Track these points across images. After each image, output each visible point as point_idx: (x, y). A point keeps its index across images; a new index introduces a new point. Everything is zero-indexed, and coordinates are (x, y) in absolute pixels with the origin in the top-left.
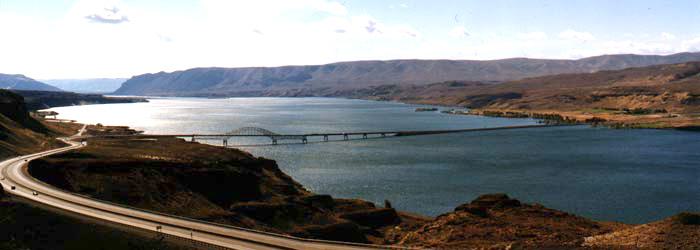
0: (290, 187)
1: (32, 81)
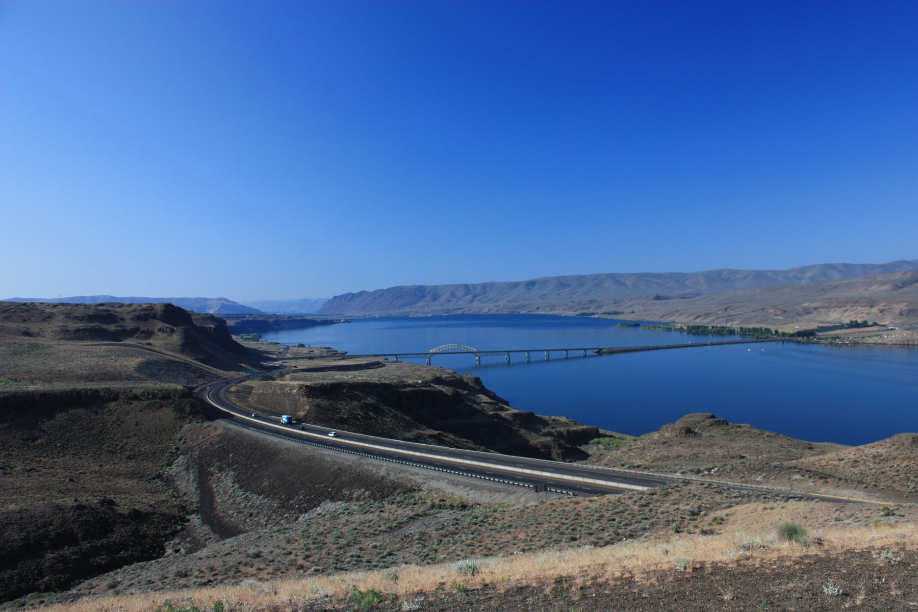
1: (233, 305)
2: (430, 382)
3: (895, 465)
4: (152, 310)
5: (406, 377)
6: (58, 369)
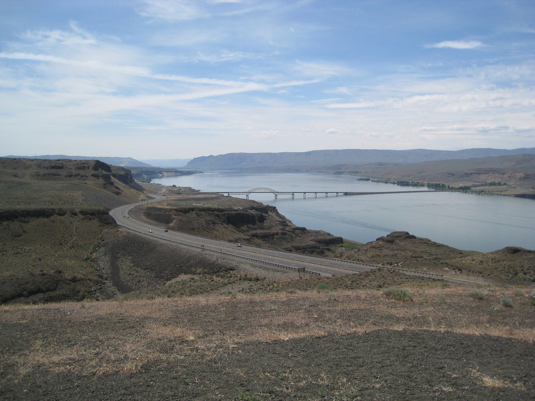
0: (284, 222)
1: (136, 162)
2: (247, 209)
3: (503, 264)
4: (87, 164)
5: (234, 206)
6: (33, 196)
